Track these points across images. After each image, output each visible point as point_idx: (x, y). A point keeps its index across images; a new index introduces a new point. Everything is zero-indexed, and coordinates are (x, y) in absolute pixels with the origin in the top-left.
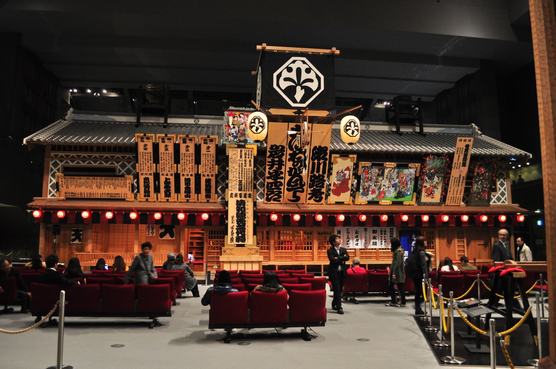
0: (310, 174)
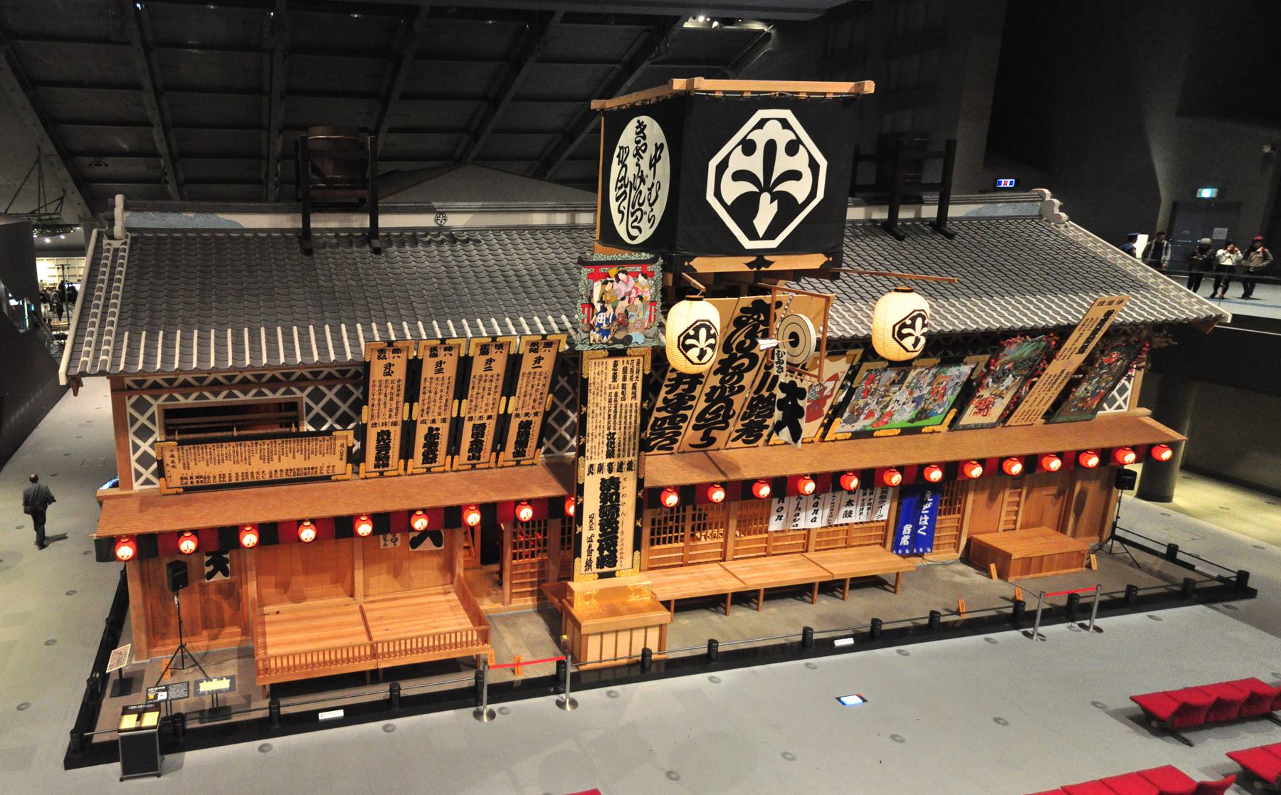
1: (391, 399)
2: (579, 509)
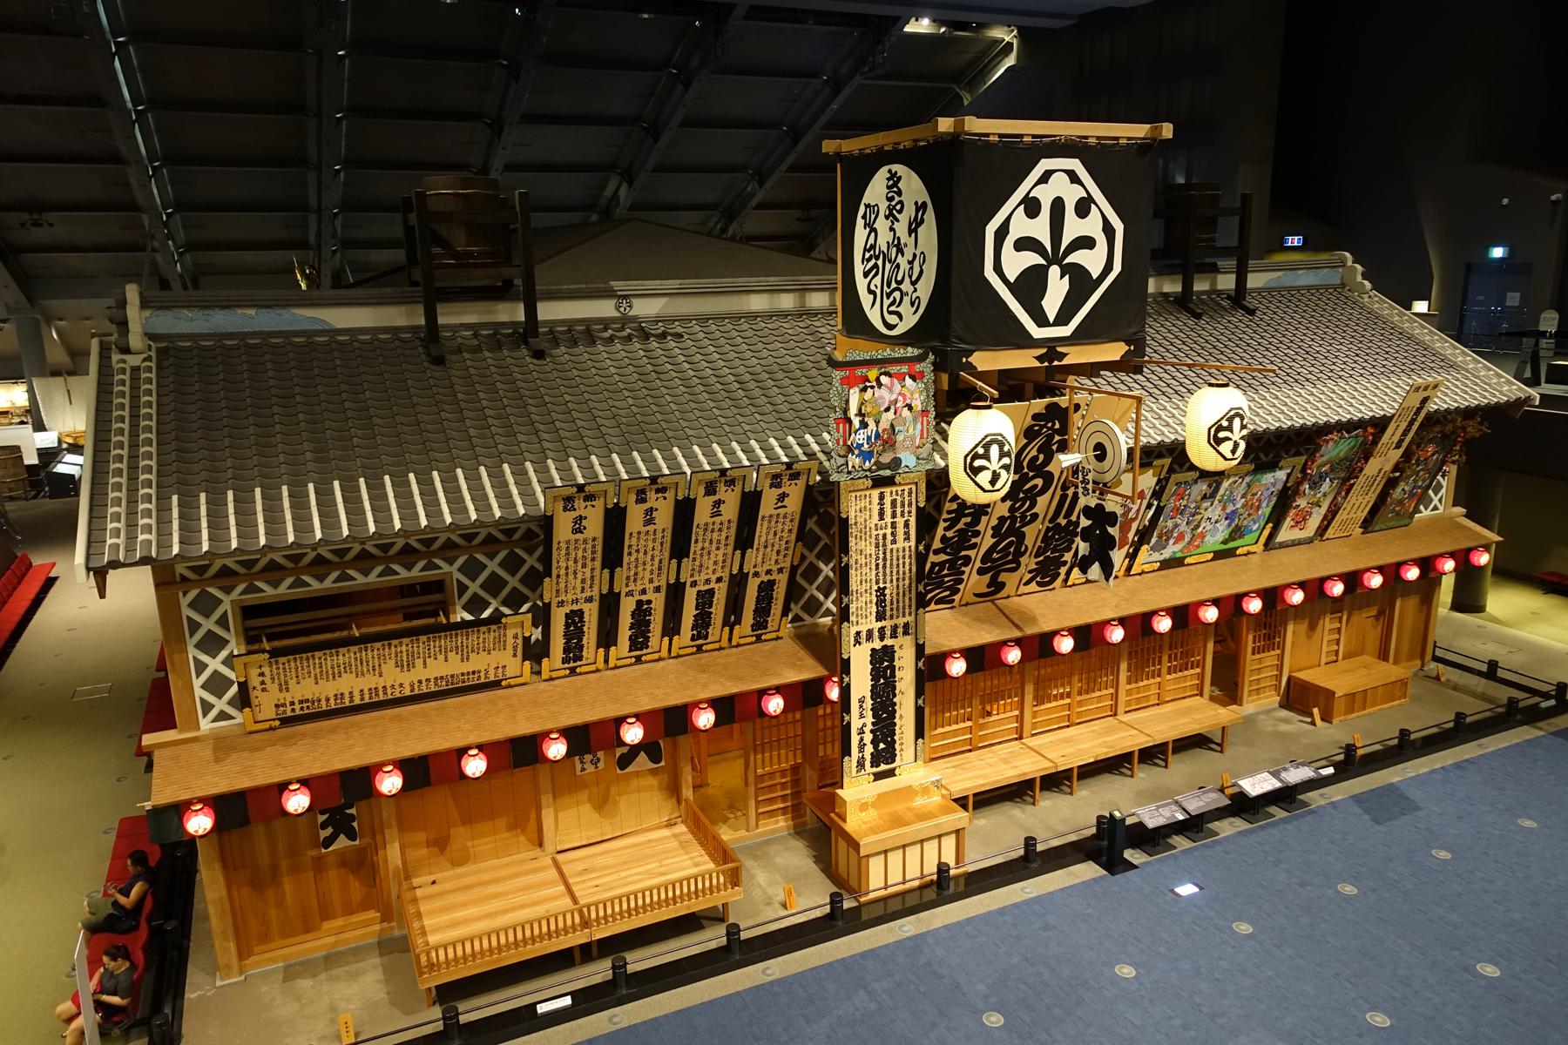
1: (584, 566)
2: (845, 692)
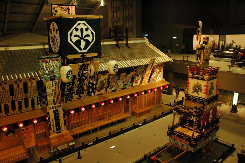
0: (87, 85)
2: (49, 118)
